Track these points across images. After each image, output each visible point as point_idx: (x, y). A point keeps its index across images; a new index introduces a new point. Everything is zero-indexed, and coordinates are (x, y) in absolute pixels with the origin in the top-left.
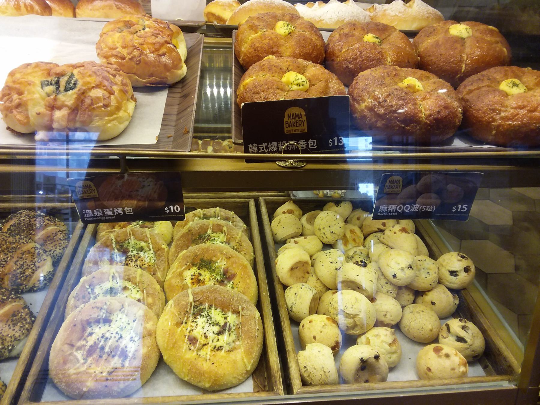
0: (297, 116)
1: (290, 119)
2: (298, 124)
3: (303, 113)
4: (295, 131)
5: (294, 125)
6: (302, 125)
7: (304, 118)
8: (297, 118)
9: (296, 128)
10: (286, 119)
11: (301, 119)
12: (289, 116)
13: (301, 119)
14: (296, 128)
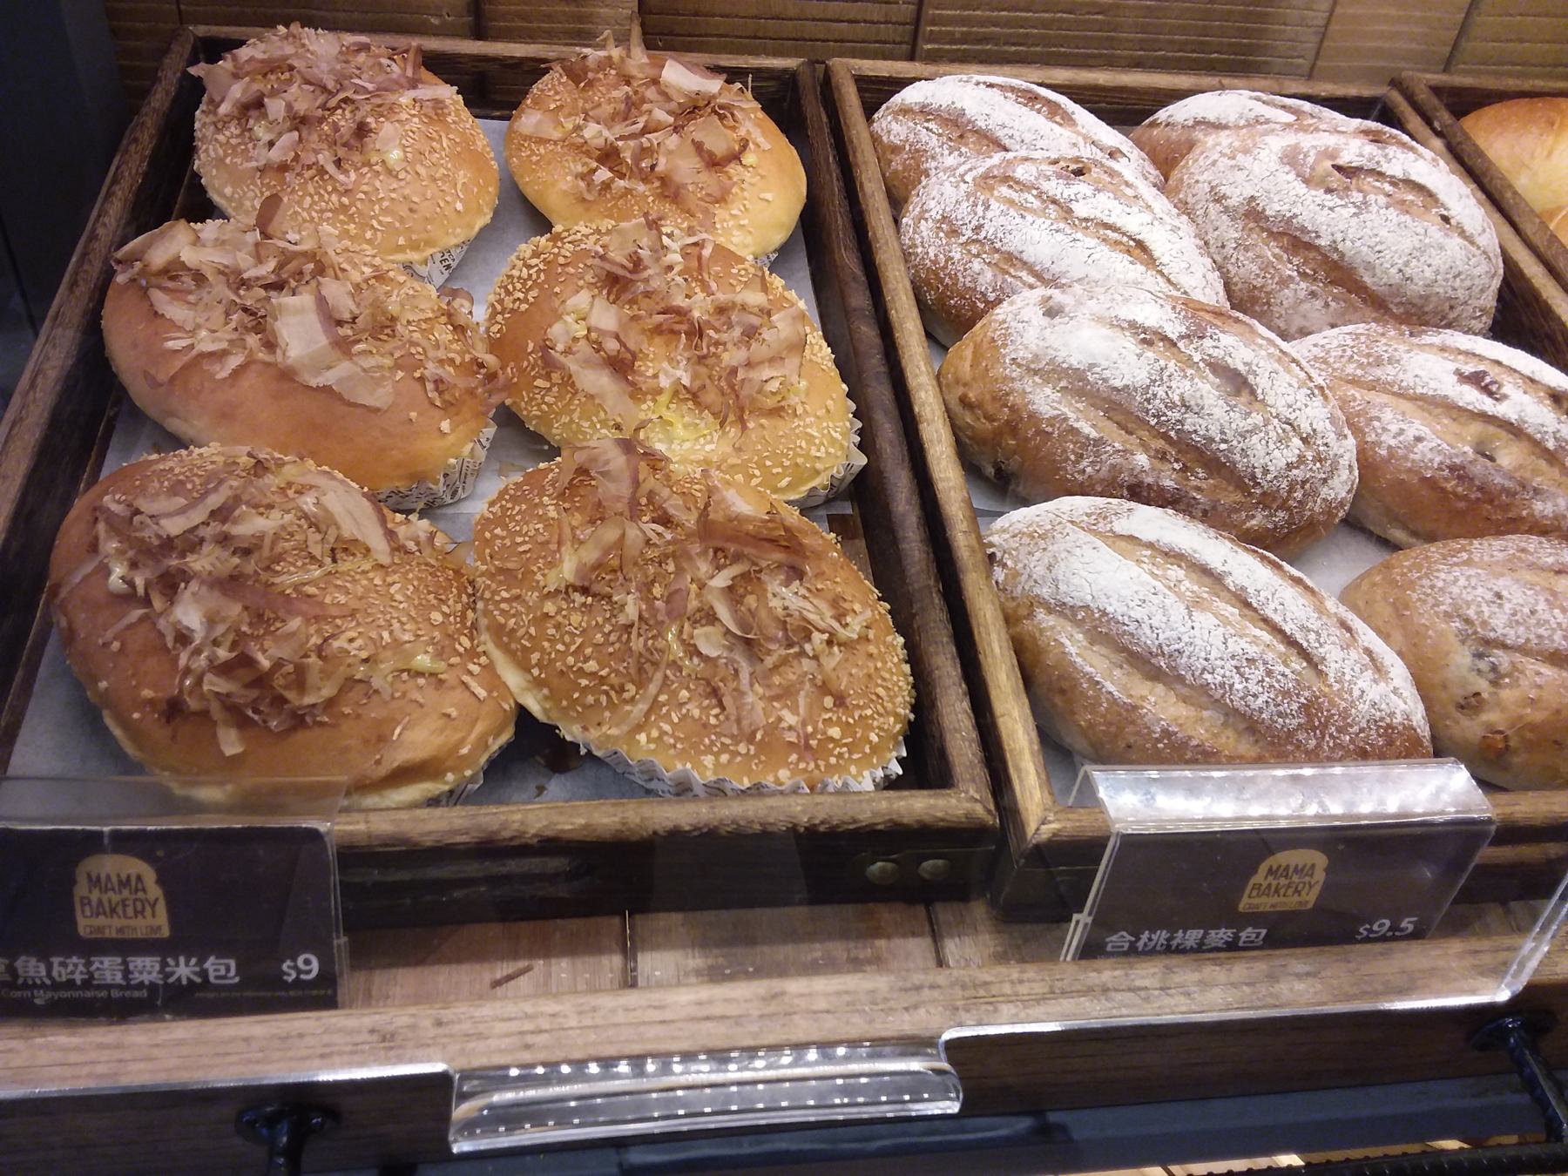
0: (124, 883)
2: (130, 911)
4: (120, 930)
5: (113, 911)
6: (148, 910)
9: (124, 922)
14: (124, 922)
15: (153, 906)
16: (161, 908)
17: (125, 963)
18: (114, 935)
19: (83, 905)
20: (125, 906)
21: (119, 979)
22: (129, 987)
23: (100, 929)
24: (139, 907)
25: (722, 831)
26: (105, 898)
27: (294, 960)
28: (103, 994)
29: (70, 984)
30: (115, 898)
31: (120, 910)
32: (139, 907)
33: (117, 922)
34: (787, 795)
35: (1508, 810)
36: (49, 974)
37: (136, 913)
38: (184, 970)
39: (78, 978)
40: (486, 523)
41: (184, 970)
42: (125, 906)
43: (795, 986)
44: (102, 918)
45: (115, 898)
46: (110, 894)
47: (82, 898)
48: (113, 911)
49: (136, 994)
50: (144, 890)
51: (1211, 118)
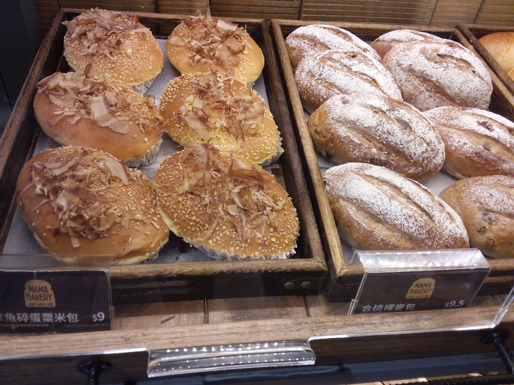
0: (41, 289)
2: (43, 298)
3: (49, 286)
4: (39, 305)
5: (37, 298)
6: (49, 298)
7: (51, 292)
9: (41, 302)
10: (27, 291)
11: (46, 293)
14: (41, 302)
15: (50, 297)
16: (53, 297)
17: (41, 315)
18: (37, 306)
19: (27, 296)
20: (41, 297)
21: (39, 320)
22: (42, 323)
23: (33, 304)
24: (46, 297)
26: (34, 294)
27: (96, 314)
28: (34, 325)
29: (23, 322)
30: (38, 294)
31: (39, 298)
32: (46, 297)
33: (38, 302)
36: (16, 319)
37: (45, 299)
38: (60, 318)
39: (26, 320)
40: (159, 171)
41: (60, 318)
42: (41, 297)
43: (261, 323)
44: (33, 300)
45: (38, 294)
46: (36, 293)
47: (27, 294)
49: (45, 325)
50: (47, 291)
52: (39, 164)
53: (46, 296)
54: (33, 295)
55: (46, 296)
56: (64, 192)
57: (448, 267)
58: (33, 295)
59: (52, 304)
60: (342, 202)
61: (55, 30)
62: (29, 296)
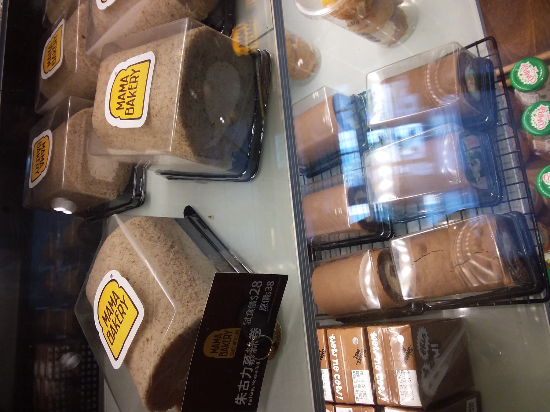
0: (216, 341)
1: (217, 351)
2: (228, 340)
3: (216, 333)
5: (226, 345)
7: (222, 331)
8: (221, 341)
10: (216, 356)
11: (222, 336)
12: (214, 351)
13: (222, 336)
15: (228, 332)
16: (229, 330)
18: (236, 346)
20: (225, 341)
23: (233, 351)
24: (133, 80)
25: (368, 221)
30: (222, 344)
31: (226, 343)
32: (133, 80)
33: (231, 345)
34: (480, 44)
35: (402, 355)
37: (229, 338)
40: (198, 95)
42: (225, 341)
43: (455, 153)
44: (228, 349)
45: (222, 344)
46: (220, 346)
47: (220, 355)
48: (133, 96)
50: (220, 335)
51: (449, 53)
52: (474, 223)
53: (226, 337)
54: (222, 350)
55: (226, 337)
56: (368, 204)
57: (339, 102)
58: (222, 350)
59: (236, 331)
60: (515, 90)
61: (378, 351)
62: (222, 353)
